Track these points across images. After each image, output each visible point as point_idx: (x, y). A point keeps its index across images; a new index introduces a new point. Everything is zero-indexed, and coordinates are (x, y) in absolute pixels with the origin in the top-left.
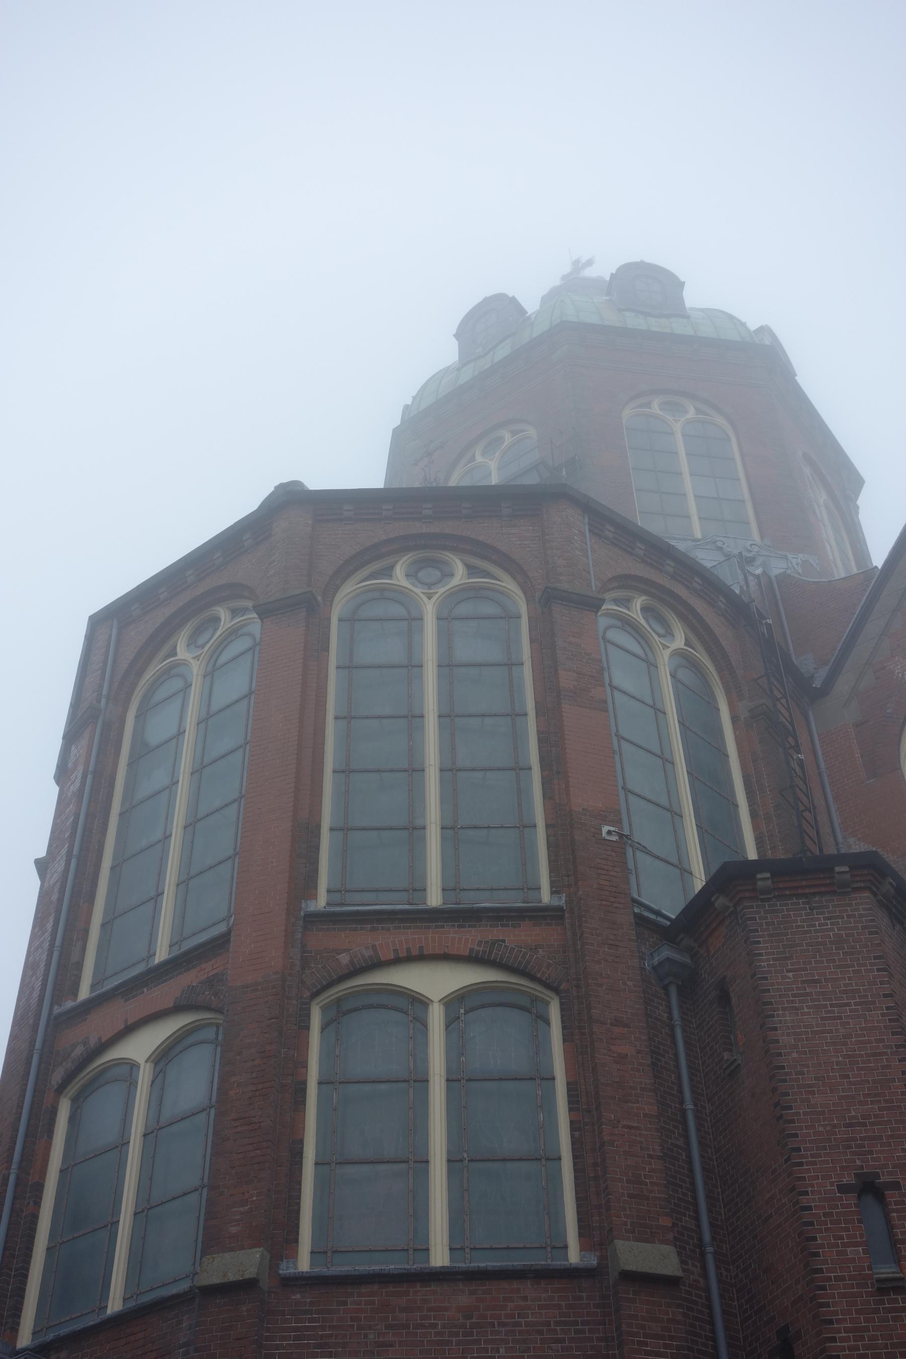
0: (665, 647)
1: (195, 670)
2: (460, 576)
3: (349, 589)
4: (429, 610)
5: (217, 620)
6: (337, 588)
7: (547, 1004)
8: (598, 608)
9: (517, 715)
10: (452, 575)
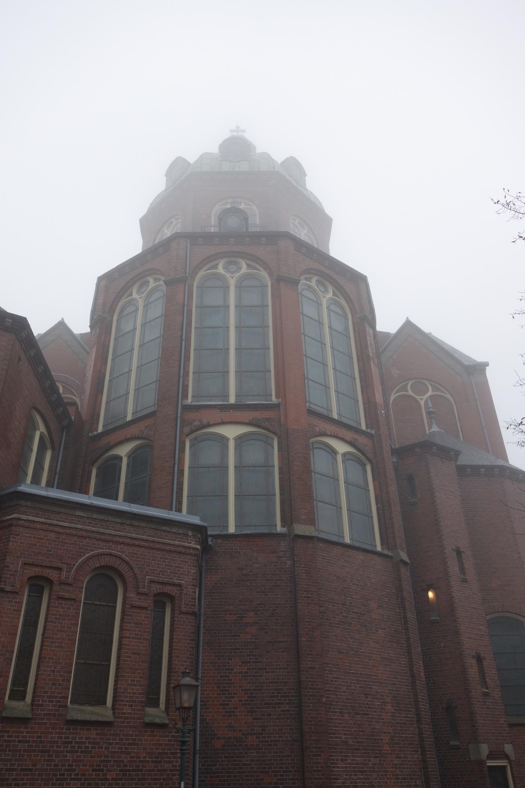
0: (324, 297)
1: (140, 303)
2: (244, 269)
3: (202, 273)
4: (232, 283)
5: (148, 282)
6: (197, 273)
7: (273, 439)
8: (298, 283)
9: (266, 349)
10: (241, 268)
